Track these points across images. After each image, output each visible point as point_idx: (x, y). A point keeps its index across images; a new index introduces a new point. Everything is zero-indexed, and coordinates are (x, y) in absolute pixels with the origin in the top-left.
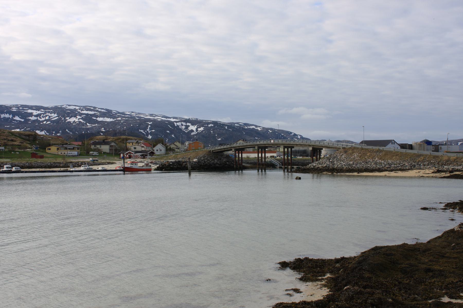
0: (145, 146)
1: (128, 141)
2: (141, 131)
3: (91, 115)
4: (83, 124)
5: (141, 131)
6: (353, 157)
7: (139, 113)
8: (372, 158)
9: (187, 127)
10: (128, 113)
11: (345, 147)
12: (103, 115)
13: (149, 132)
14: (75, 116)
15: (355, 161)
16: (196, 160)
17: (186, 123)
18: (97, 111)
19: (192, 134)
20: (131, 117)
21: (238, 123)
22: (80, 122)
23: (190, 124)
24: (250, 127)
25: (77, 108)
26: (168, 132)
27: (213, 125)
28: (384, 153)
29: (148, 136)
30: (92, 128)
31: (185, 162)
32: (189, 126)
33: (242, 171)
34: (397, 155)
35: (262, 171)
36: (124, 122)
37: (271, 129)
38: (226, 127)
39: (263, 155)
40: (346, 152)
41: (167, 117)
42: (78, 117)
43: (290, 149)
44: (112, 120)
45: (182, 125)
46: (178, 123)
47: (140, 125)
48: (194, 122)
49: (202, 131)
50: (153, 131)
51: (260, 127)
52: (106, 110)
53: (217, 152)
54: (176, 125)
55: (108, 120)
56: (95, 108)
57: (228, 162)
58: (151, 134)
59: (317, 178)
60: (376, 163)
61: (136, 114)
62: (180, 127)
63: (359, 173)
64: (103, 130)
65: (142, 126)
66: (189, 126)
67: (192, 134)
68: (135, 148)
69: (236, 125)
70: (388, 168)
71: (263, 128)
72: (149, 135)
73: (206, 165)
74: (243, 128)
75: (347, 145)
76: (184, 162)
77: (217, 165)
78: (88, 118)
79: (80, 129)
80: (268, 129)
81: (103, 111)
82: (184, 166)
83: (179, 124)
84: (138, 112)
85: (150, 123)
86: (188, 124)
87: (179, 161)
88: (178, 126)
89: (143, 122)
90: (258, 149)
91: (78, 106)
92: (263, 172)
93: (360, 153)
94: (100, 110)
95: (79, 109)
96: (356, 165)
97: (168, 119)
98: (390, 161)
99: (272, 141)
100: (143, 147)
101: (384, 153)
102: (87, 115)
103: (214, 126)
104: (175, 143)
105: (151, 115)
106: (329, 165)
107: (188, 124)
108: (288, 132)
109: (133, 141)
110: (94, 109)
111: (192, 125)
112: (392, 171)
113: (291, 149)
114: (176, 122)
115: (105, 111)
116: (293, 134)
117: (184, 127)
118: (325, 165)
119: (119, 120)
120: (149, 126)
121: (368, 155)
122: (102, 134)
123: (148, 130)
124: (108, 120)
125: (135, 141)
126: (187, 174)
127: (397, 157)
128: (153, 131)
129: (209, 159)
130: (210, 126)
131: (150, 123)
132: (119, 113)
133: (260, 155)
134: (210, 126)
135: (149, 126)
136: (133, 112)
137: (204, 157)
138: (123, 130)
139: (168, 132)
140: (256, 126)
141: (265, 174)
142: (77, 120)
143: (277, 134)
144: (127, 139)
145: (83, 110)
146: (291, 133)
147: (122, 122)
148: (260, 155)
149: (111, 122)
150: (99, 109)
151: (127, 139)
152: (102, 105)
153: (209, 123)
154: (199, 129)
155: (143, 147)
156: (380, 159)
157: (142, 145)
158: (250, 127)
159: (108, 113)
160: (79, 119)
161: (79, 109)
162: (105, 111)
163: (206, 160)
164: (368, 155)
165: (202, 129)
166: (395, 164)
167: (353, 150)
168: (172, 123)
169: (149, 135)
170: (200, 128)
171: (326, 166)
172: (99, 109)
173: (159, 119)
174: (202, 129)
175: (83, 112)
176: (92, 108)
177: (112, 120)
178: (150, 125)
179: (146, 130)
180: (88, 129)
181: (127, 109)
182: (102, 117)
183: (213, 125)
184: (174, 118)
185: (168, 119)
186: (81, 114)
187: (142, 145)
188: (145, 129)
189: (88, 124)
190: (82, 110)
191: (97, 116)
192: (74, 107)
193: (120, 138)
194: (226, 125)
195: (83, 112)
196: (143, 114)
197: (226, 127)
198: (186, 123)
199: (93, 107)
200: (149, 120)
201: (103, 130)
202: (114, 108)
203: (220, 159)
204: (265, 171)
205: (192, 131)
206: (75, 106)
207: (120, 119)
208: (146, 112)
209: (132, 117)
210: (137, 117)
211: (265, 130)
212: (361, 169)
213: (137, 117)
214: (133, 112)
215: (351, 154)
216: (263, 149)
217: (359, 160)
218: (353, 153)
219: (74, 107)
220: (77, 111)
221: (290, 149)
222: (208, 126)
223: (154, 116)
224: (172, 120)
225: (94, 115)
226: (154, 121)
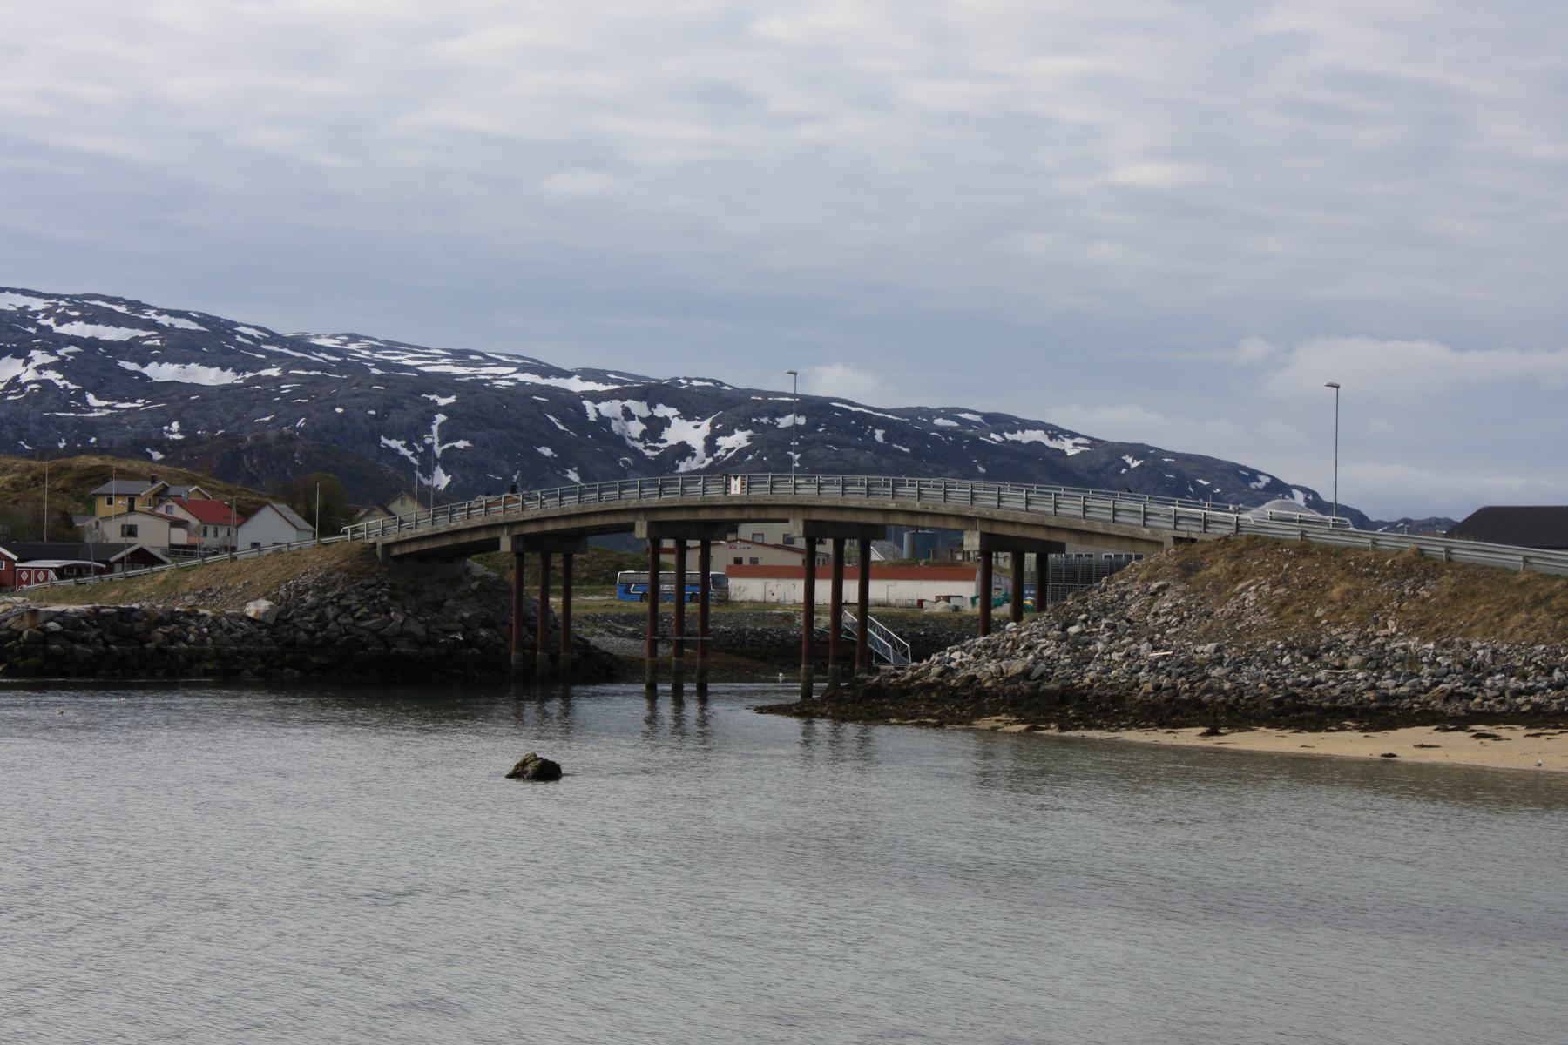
0: (194, 522)
1: (113, 486)
2: (394, 443)
3: (111, 346)
4: (63, 399)
5: (394, 443)
6: (1231, 608)
7: (391, 345)
8: (1361, 623)
9: (656, 427)
10: (329, 343)
11: (1194, 530)
12: (182, 347)
13: (438, 450)
14: (22, 353)
15: (1239, 635)
16: (264, 605)
17: (652, 406)
18: (151, 325)
19: (683, 467)
20: (344, 367)
21: (949, 413)
22: (46, 384)
23: (671, 412)
24: (1018, 436)
25: (37, 304)
26: (547, 451)
27: (802, 421)
28: (1447, 583)
29: (428, 473)
30: (114, 421)
31: (173, 617)
32: (666, 422)
33: (566, 697)
34: (1537, 602)
35: (678, 697)
36: (295, 393)
37: (1140, 451)
38: (879, 435)
39: (851, 590)
40: (1187, 570)
41: (547, 371)
42: (39, 357)
43: (1030, 558)
44: (228, 377)
45: (628, 415)
46: (603, 406)
47: (387, 409)
48: (694, 402)
49: (743, 452)
50: (461, 444)
51: (1073, 435)
52: (203, 319)
53: (421, 557)
54: (592, 416)
55: (210, 376)
56: (137, 306)
57: (487, 624)
58: (448, 461)
59: (834, 759)
60: (1376, 663)
61: (374, 349)
62: (615, 426)
63: (1213, 732)
64: (174, 431)
65: (395, 416)
66: (666, 422)
67: (683, 467)
68: (130, 531)
69: (939, 422)
70: (1450, 696)
71: (1095, 443)
72: (439, 471)
73: (329, 641)
74: (974, 441)
75: (1206, 523)
76: (160, 622)
77: (403, 647)
78: (95, 366)
79: (43, 422)
80: (1117, 450)
81: (181, 324)
82: (159, 650)
83: (610, 408)
84: (383, 336)
85: (442, 402)
86: (662, 411)
87: (126, 615)
88: (604, 421)
89: (404, 395)
90: (656, 542)
91: (39, 295)
92: (692, 708)
93: (1284, 581)
94: (164, 320)
95: (48, 313)
96: (1237, 667)
97: (553, 382)
98: (1481, 649)
99: (736, 486)
100: (177, 523)
101: (1447, 583)
102: (91, 344)
103: (811, 427)
104: (395, 507)
105: (460, 356)
106: (1052, 663)
107: (662, 411)
108: (1235, 469)
109: (131, 486)
110: (135, 313)
111: (687, 415)
112: (1461, 723)
113: (1042, 561)
114: (596, 397)
115: (194, 326)
116: (1265, 480)
117: (636, 428)
118: (1017, 666)
119: (269, 379)
120: (441, 418)
121: (1335, 593)
122: (157, 456)
123: (433, 438)
124: (210, 376)
125: (147, 489)
126: (641, 707)
127: (1542, 616)
128: (461, 444)
129: (353, 600)
130: (785, 422)
131: (442, 402)
132: (274, 338)
133: (824, 590)
134: (785, 422)
135: (441, 418)
136: (355, 338)
137: (323, 586)
138: (282, 438)
139: (547, 451)
140: (1054, 432)
141: (703, 721)
142: (28, 375)
143: (924, 444)
144: (102, 475)
145: (71, 320)
146: (1254, 474)
147: (286, 388)
148: (824, 590)
149: (225, 389)
150: (161, 312)
151: (102, 475)
152: (177, 294)
153: (780, 410)
154: (721, 441)
155: (177, 523)
156: (1417, 627)
157: (179, 513)
158: (1018, 436)
159: (213, 339)
160: (40, 369)
161: (48, 313)
162: (194, 326)
163: (330, 612)
164: (1335, 593)
165: (739, 439)
166: (1510, 671)
167: (1239, 556)
168: (569, 405)
169: (439, 471)
170: (729, 433)
171: (1026, 674)
172: (161, 312)
173: (503, 376)
174: (739, 439)
175: (66, 329)
176: (122, 309)
177: (228, 377)
178: (446, 410)
179: (421, 441)
180: (91, 426)
181: (324, 321)
182: (173, 362)
183: (802, 421)
184: (587, 375)
185: (553, 382)
186: (52, 342)
187: (179, 513)
188: (412, 436)
189: (91, 399)
190: (63, 319)
191: (143, 355)
192: (21, 301)
193: (69, 468)
194: (881, 423)
195: (66, 329)
196: (411, 348)
197: (879, 435)
198: (652, 406)
199: (129, 303)
200: (445, 384)
201: (174, 431)
202: (250, 314)
203: (438, 606)
204: (703, 696)
205: (684, 450)
206: (25, 293)
207: (274, 372)
208: (429, 332)
209: (349, 366)
210: (378, 365)
211: (1104, 458)
212: (1257, 699)
213: (378, 365)
214: (355, 338)
215: (1221, 588)
216: (839, 541)
217: (1268, 629)
218: (1236, 576)
219: (21, 301)
220: (34, 323)
221: (1030, 558)
222: (774, 427)
223: (476, 364)
224: (575, 385)
225: (134, 350)
226: (473, 388)
